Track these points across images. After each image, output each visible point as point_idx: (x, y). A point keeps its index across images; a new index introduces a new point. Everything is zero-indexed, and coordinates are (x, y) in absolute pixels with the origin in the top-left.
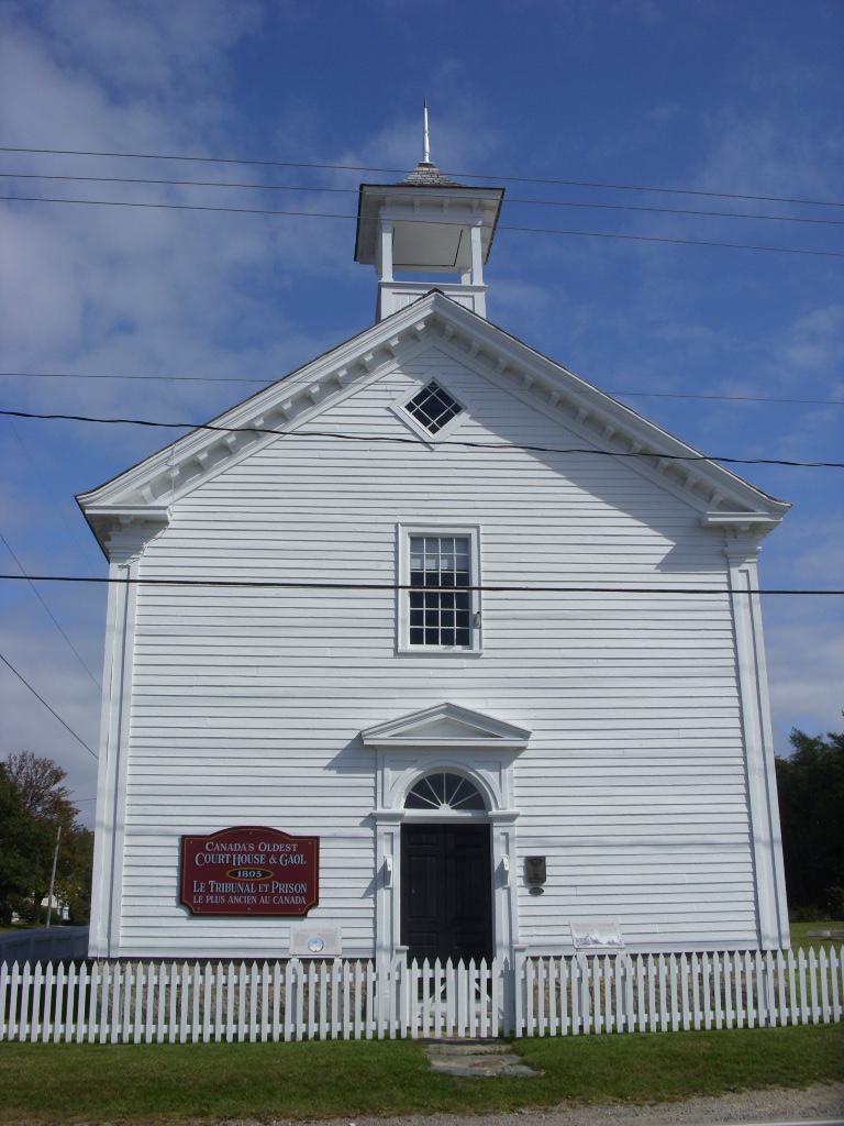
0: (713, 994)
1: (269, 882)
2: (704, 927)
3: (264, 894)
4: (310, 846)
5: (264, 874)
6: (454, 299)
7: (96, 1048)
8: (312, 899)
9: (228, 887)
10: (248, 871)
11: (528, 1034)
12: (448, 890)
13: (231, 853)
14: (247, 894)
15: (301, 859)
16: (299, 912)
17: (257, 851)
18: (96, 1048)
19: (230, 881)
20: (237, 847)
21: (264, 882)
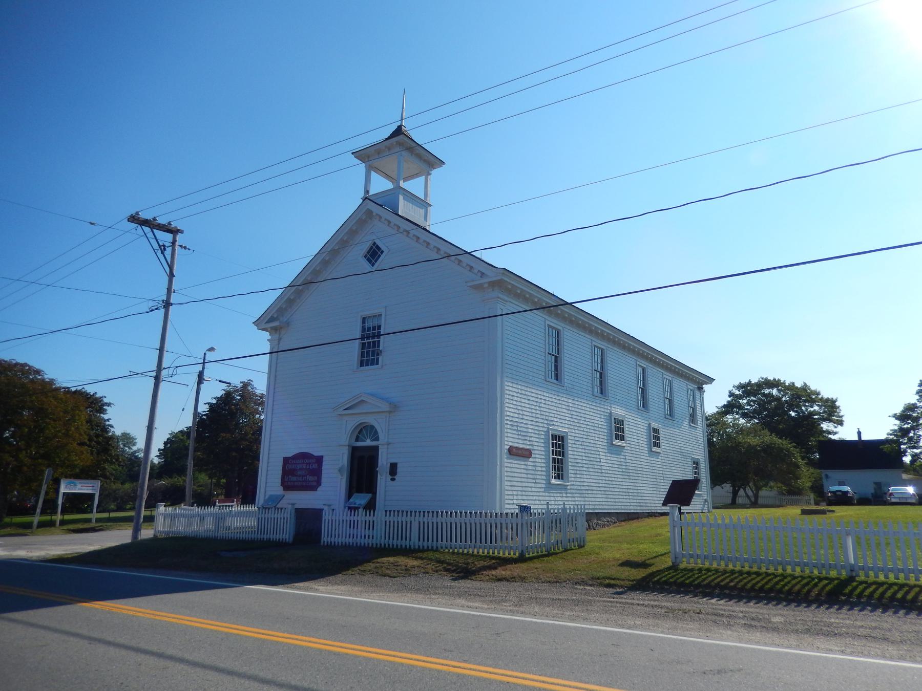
8: (319, 483)
12: (363, 470)
15: (315, 466)
16: (314, 488)
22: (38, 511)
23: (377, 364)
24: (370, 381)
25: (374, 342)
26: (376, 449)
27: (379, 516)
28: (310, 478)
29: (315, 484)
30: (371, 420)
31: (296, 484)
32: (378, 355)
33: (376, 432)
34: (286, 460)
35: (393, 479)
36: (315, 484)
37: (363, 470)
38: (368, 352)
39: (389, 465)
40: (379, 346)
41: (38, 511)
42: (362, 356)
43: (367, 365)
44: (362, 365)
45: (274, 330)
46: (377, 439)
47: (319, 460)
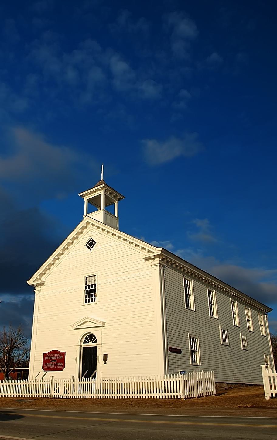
0: (39, 388)
1: (56, 363)
2: (229, 380)
3: (56, 366)
4: (64, 354)
5: (56, 361)
6: (118, 244)
7: (137, 399)
8: (64, 367)
9: (50, 364)
10: (54, 361)
11: (274, 396)
12: (89, 361)
13: (51, 356)
14: (53, 366)
15: (62, 357)
16: (61, 370)
17: (55, 356)
18: (114, 400)
19: (50, 363)
20: (52, 355)
21: (56, 363)
22: (93, 287)
23: (95, 301)
24: (93, 312)
25: (92, 290)
26: (95, 348)
27: (97, 382)
28: (59, 364)
29: (61, 367)
30: (93, 331)
31: (51, 367)
32: (95, 296)
33: (95, 338)
34: (45, 355)
35: (105, 363)
36: (62, 367)
37: (89, 361)
38: (89, 295)
39: (103, 355)
40: (95, 292)
41: (93, 287)
42: (86, 297)
43: (89, 302)
44: (86, 302)
45: (219, 392)
46: (96, 342)
47: (64, 354)
